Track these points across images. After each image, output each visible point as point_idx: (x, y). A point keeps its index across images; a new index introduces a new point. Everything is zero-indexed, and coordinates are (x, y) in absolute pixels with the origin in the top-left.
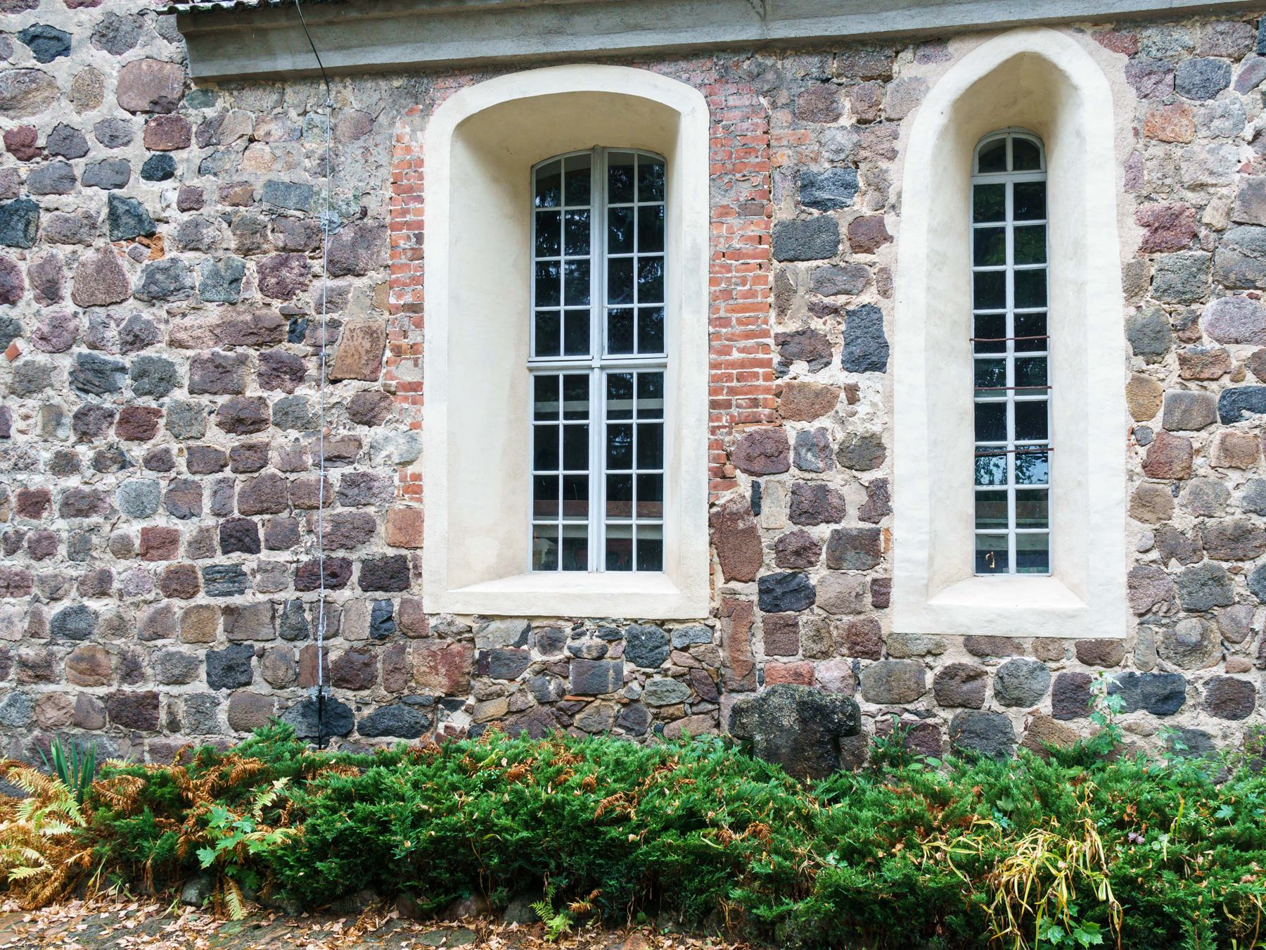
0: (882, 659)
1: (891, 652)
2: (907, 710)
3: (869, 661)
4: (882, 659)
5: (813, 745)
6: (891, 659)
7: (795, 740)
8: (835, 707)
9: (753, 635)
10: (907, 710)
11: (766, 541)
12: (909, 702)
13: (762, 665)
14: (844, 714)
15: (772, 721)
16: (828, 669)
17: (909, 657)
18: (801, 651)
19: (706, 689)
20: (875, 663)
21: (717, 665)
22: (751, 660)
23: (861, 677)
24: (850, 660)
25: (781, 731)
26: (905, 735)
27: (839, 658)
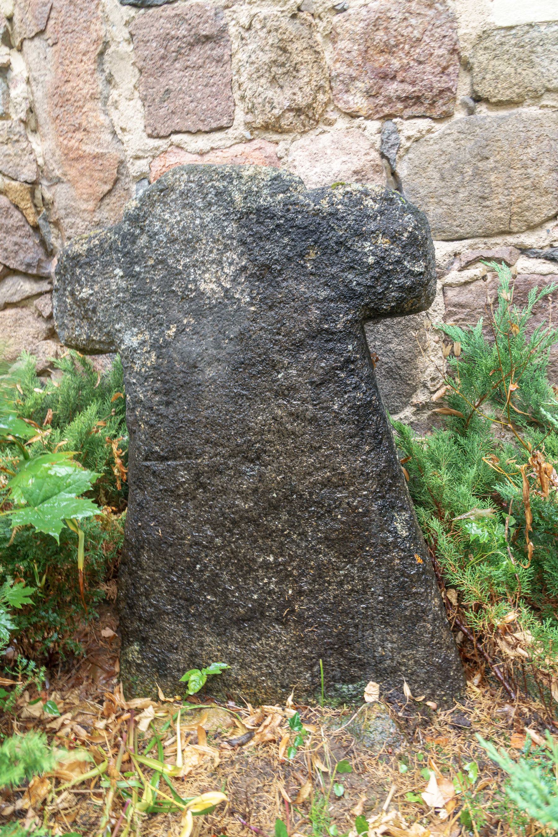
0: (460, 115)
1: (484, 90)
2: (524, 250)
3: (424, 124)
4: (460, 115)
5: (299, 345)
6: (482, 110)
7: (241, 337)
8: (365, 216)
9: (109, 81)
10: (524, 250)
11: (355, 828)
12: (532, 228)
13: (141, 166)
14: (394, 238)
15: (166, 283)
16: (315, 157)
17: (537, 97)
18: (240, 116)
19: (9, 242)
20: (440, 128)
21: (28, 174)
22: (113, 152)
23: (403, 170)
24: (373, 126)
25: (198, 314)
26: (526, 313)
27: (342, 123)
